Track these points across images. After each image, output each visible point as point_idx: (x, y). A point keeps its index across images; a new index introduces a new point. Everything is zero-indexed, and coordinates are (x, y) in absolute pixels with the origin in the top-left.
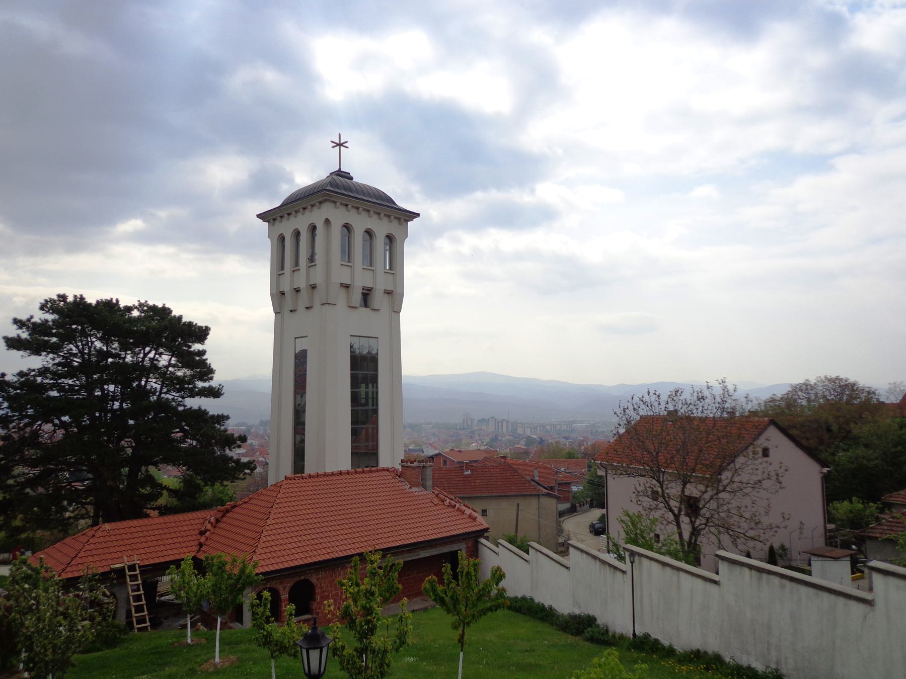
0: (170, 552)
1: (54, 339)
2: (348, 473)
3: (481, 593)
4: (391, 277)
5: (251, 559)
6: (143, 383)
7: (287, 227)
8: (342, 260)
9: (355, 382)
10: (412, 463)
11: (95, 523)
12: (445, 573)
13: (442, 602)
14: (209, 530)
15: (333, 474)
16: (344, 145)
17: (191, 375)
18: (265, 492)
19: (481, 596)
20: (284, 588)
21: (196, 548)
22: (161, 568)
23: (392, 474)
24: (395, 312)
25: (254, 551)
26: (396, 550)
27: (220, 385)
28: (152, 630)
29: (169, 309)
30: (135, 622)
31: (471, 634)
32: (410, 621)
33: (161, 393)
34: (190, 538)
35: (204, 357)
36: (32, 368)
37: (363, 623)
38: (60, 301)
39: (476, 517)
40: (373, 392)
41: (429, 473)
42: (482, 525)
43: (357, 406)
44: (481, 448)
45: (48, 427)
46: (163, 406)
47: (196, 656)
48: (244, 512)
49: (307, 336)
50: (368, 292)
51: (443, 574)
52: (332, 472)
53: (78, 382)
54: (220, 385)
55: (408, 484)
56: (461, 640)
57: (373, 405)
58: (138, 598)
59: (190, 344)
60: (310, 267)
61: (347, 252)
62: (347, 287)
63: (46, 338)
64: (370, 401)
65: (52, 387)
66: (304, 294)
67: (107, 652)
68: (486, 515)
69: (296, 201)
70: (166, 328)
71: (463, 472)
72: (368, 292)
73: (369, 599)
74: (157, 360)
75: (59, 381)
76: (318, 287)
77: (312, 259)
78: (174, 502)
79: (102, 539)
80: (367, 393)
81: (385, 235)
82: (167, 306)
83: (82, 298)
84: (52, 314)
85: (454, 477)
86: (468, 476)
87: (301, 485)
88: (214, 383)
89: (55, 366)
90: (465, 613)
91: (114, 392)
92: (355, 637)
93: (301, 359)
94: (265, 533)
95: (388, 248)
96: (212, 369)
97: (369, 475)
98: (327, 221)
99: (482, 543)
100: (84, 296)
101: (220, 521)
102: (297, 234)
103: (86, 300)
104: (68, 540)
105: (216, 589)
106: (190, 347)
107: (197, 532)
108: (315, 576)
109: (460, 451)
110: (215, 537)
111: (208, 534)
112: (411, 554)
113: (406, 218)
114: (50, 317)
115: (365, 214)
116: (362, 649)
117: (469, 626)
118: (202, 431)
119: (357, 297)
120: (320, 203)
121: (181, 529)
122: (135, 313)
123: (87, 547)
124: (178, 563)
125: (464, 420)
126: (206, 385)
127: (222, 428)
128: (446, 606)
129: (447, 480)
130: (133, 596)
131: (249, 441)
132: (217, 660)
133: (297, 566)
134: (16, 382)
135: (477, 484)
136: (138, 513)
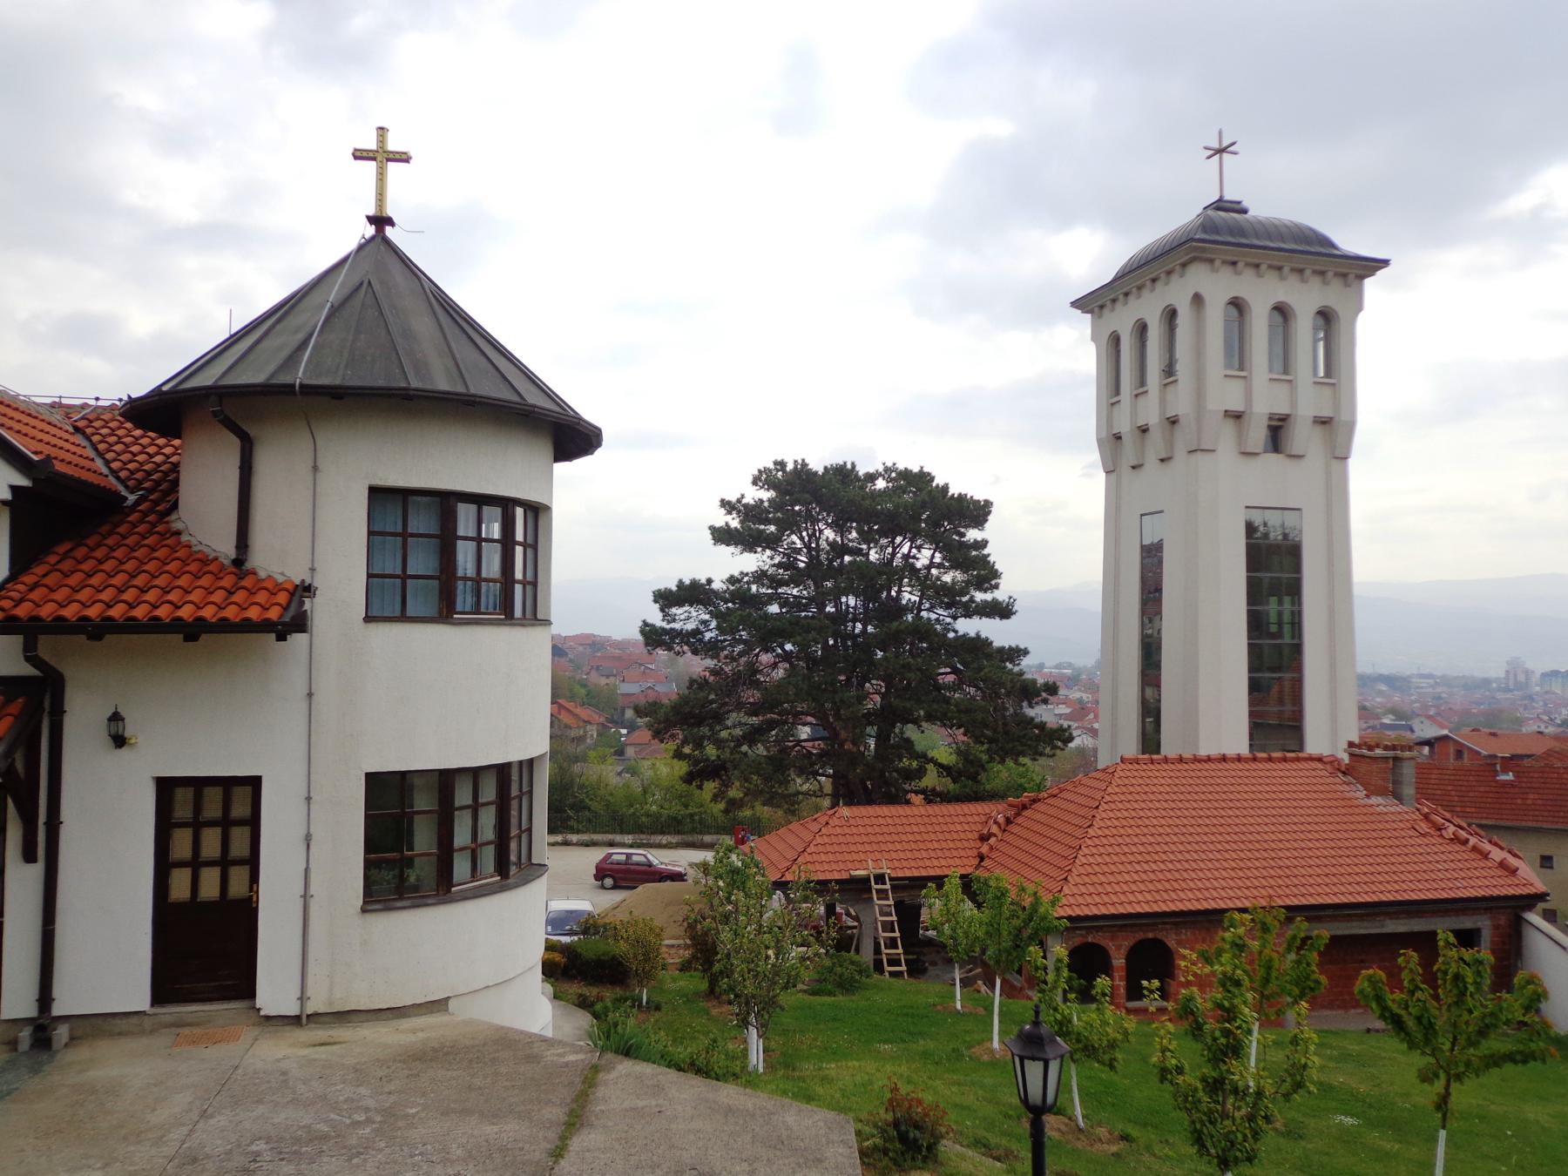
0: (936, 863)
1: (772, 528)
2: (1239, 759)
3: (1487, 1021)
4: (1327, 391)
5: (1060, 891)
6: (893, 593)
7: (1123, 320)
8: (1228, 366)
9: (1255, 593)
10: (1370, 748)
11: (834, 805)
12: (1406, 967)
13: (1397, 1023)
14: (995, 835)
15: (1209, 759)
16: (1212, 152)
17: (963, 581)
18: (1085, 781)
19: (1487, 1026)
20: (1118, 948)
21: (975, 862)
22: (919, 883)
23: (1328, 767)
24: (1294, 456)
25: (1066, 879)
26: (1315, 913)
27: (1010, 598)
28: (911, 979)
29: (929, 474)
30: (885, 961)
31: (1465, 1096)
32: (1312, 1048)
33: (920, 610)
34: (966, 844)
35: (985, 552)
36: (745, 572)
37: (1217, 1034)
38: (778, 471)
39: (1518, 869)
40: (1293, 613)
41: (1408, 771)
42: (1531, 885)
43: (1259, 638)
44: (1546, 731)
45: (766, 658)
46: (923, 631)
47: (966, 1032)
48: (1052, 811)
49: (1162, 512)
50: (1280, 423)
51: (1401, 969)
52: (1208, 756)
53: (805, 592)
54: (1010, 598)
55: (1361, 788)
56: (1442, 1103)
57: (1293, 638)
58: (889, 927)
59: (962, 530)
60: (1166, 385)
61: (1238, 355)
62: (1237, 416)
63: (762, 527)
64: (1287, 629)
65: (771, 599)
66: (1155, 435)
67: (841, 999)
68: (1551, 867)
69: (1139, 267)
70: (924, 506)
71: (1495, 776)
72: (1280, 423)
73: (1229, 991)
74: (914, 557)
75: (780, 591)
76: (1181, 421)
77: (1169, 371)
78: (947, 784)
79: (839, 830)
80: (1280, 614)
81: (1315, 308)
82: (925, 470)
83: (804, 464)
84: (768, 490)
85: (1474, 783)
86: (1505, 784)
87: (1150, 774)
88: (1000, 595)
89: (775, 569)
90: (1448, 1054)
91: (855, 608)
92: (1203, 1055)
93: (1152, 555)
94: (1086, 851)
95: (1322, 335)
96: (997, 571)
97: (1281, 766)
98: (1198, 299)
99: (1530, 923)
100: (807, 461)
101: (1012, 823)
102: (1142, 329)
103: (810, 467)
104: (794, 826)
105: (993, 931)
106: (963, 535)
107: (976, 836)
108: (1174, 937)
109: (1494, 735)
110: (1003, 847)
111: (993, 840)
112: (1365, 924)
113: (1359, 272)
114: (766, 495)
115: (1272, 275)
116: (1215, 1080)
117: (1462, 1083)
118: (982, 673)
119: (1258, 434)
120: (1184, 265)
121: (952, 827)
122: (881, 484)
123: (819, 840)
124: (939, 881)
125: (1507, 672)
126: (988, 596)
127: (1016, 669)
128: (1407, 1034)
129: (1459, 788)
130: (883, 922)
131: (1062, 692)
132: (996, 1044)
133: (1079, 916)
134: (725, 591)
135: (1529, 802)
136: (895, 798)
